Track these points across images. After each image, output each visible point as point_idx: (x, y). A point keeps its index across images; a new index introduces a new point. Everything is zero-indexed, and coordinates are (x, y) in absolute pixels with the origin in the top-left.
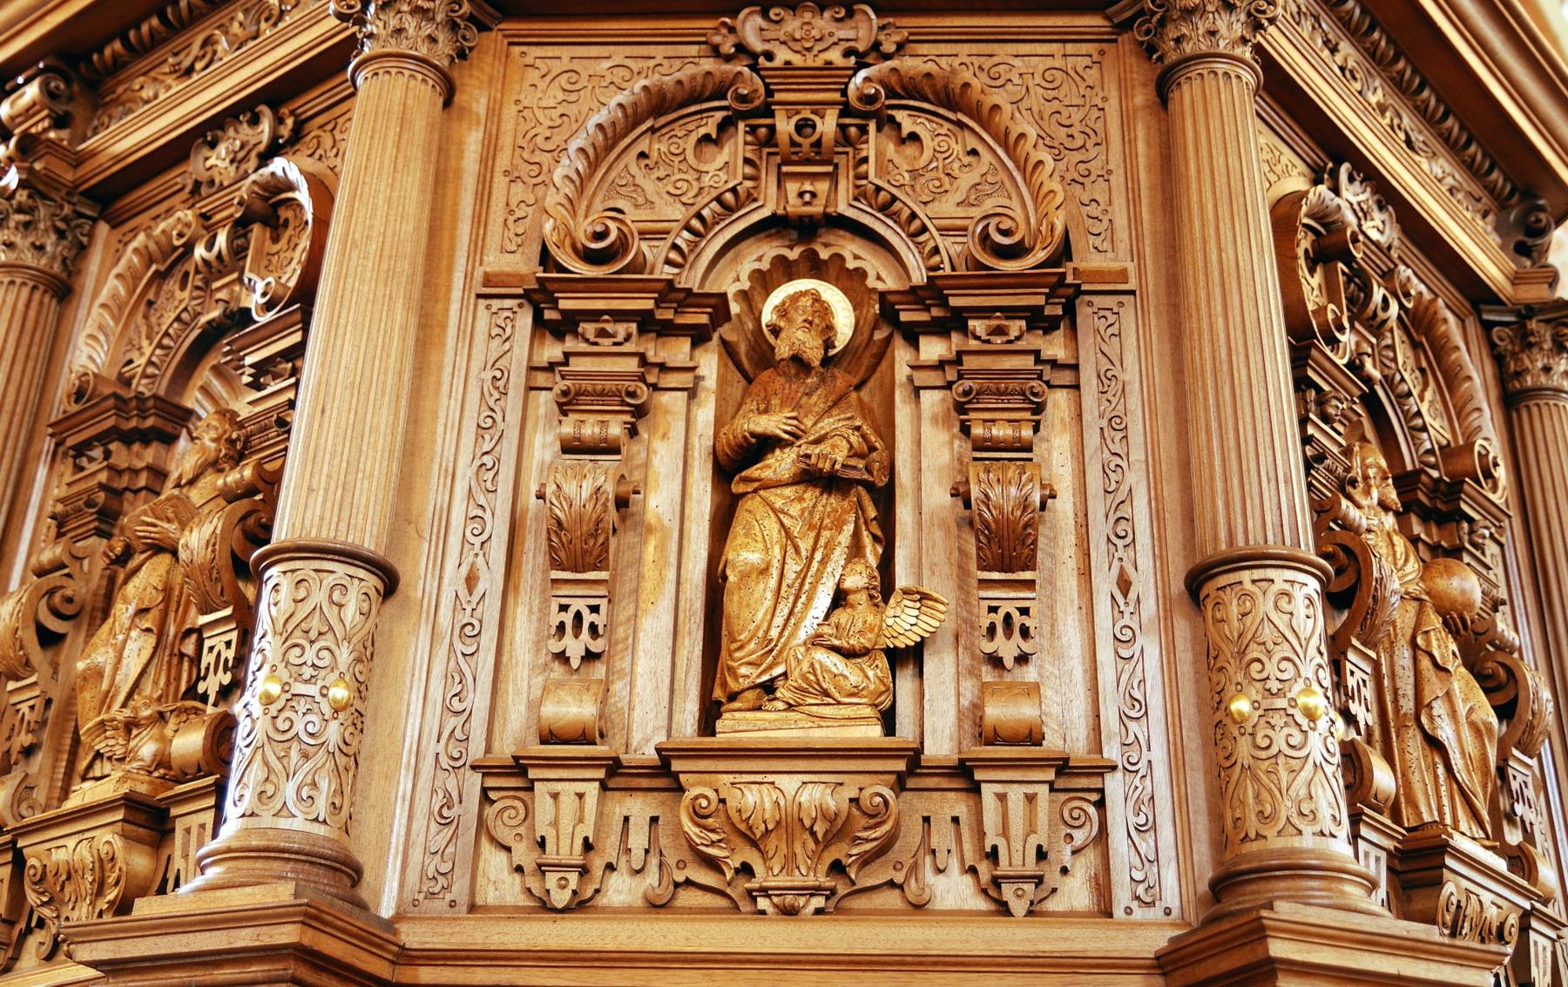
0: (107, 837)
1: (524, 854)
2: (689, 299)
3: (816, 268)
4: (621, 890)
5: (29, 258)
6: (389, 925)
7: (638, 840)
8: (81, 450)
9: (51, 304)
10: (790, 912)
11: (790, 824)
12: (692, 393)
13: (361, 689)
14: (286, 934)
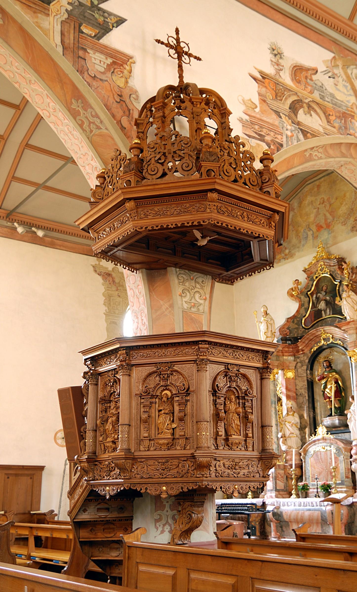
0: (111, 444)
1: (143, 446)
2: (154, 396)
3: (168, 390)
4: (152, 449)
5: (93, 383)
6: (133, 453)
7: (153, 445)
8: (102, 404)
9: (96, 386)
10: (164, 450)
11: (164, 444)
12: (156, 404)
13: (128, 435)
14: (124, 456)
